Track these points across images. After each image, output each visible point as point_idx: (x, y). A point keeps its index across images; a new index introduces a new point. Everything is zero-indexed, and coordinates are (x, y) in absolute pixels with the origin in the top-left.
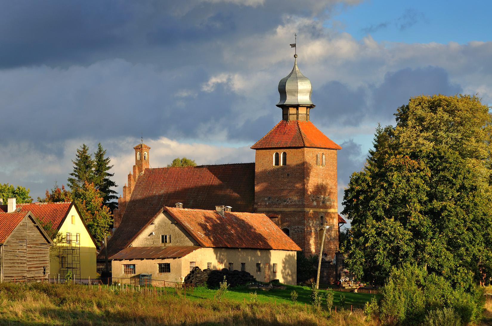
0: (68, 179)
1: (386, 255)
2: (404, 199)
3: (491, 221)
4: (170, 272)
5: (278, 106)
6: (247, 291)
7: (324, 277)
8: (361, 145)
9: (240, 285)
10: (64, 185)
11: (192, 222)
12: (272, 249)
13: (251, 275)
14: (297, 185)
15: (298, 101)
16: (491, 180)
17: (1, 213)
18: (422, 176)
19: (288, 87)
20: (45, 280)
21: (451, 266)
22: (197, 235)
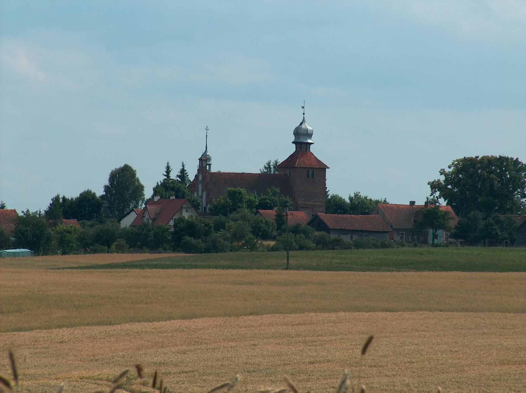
0: (64, 195)
1: (478, 159)
2: (121, 247)
3: (461, 392)
4: (415, 202)
5: (293, 143)
6: (454, 170)
7: (317, 245)
8: (440, 175)
9: (247, 223)
10: (308, 126)
11: (391, 370)
12: (307, 133)
13: (99, 192)
14: (138, 244)
15: (308, 132)
16: (313, 392)
17: (0, 210)
18: (354, 349)
19: (113, 380)
20: (199, 205)
21: (448, 341)
22: (92, 272)
